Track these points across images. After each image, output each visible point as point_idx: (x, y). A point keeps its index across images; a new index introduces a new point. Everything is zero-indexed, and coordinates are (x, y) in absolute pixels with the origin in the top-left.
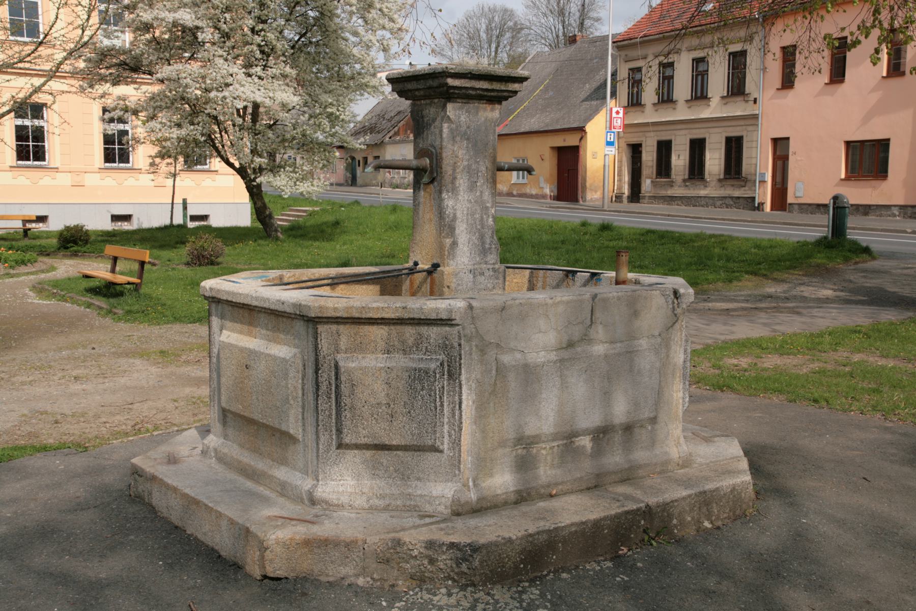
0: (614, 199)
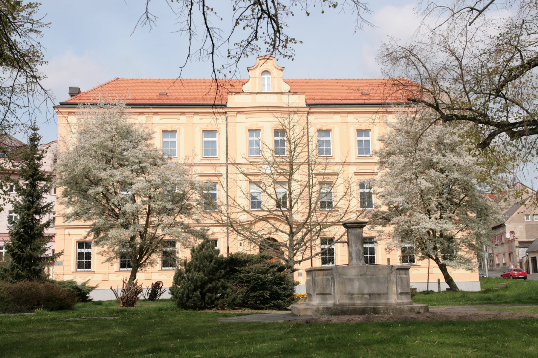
0: (368, 246)
